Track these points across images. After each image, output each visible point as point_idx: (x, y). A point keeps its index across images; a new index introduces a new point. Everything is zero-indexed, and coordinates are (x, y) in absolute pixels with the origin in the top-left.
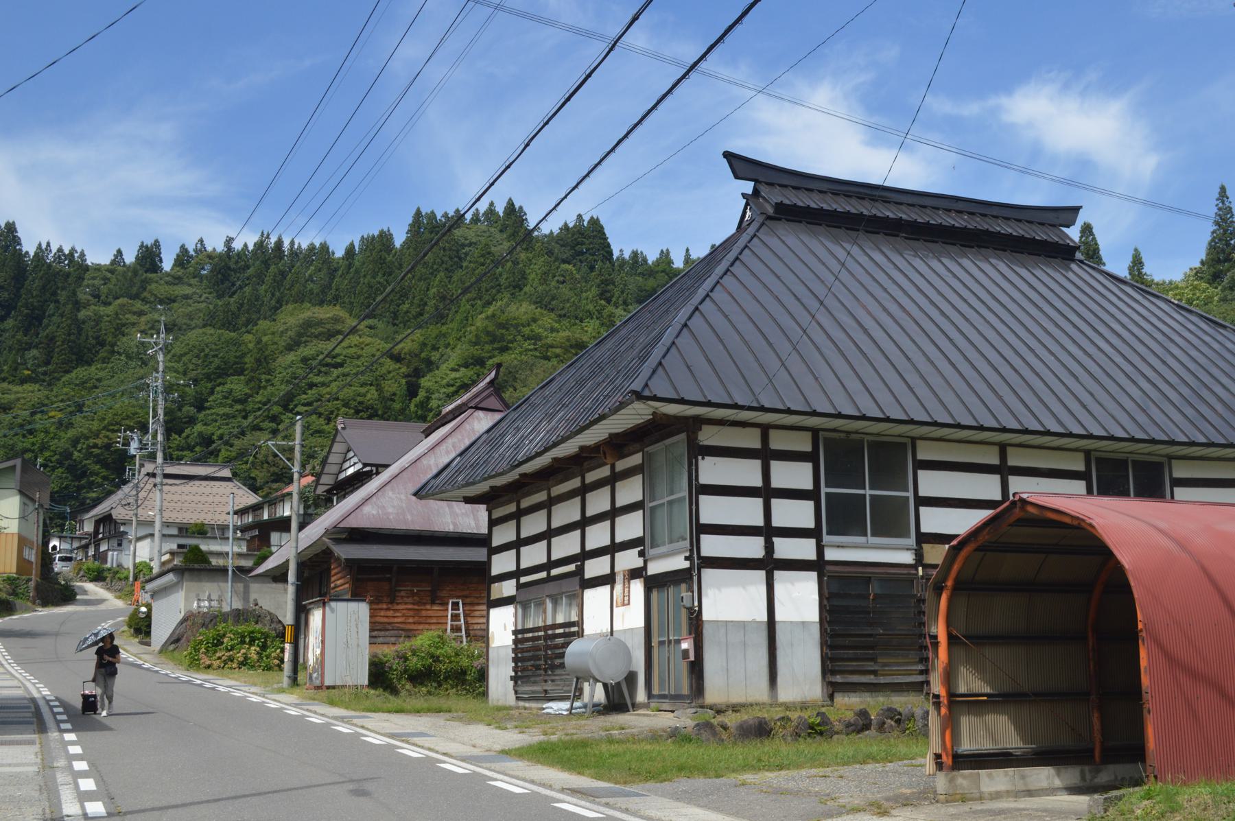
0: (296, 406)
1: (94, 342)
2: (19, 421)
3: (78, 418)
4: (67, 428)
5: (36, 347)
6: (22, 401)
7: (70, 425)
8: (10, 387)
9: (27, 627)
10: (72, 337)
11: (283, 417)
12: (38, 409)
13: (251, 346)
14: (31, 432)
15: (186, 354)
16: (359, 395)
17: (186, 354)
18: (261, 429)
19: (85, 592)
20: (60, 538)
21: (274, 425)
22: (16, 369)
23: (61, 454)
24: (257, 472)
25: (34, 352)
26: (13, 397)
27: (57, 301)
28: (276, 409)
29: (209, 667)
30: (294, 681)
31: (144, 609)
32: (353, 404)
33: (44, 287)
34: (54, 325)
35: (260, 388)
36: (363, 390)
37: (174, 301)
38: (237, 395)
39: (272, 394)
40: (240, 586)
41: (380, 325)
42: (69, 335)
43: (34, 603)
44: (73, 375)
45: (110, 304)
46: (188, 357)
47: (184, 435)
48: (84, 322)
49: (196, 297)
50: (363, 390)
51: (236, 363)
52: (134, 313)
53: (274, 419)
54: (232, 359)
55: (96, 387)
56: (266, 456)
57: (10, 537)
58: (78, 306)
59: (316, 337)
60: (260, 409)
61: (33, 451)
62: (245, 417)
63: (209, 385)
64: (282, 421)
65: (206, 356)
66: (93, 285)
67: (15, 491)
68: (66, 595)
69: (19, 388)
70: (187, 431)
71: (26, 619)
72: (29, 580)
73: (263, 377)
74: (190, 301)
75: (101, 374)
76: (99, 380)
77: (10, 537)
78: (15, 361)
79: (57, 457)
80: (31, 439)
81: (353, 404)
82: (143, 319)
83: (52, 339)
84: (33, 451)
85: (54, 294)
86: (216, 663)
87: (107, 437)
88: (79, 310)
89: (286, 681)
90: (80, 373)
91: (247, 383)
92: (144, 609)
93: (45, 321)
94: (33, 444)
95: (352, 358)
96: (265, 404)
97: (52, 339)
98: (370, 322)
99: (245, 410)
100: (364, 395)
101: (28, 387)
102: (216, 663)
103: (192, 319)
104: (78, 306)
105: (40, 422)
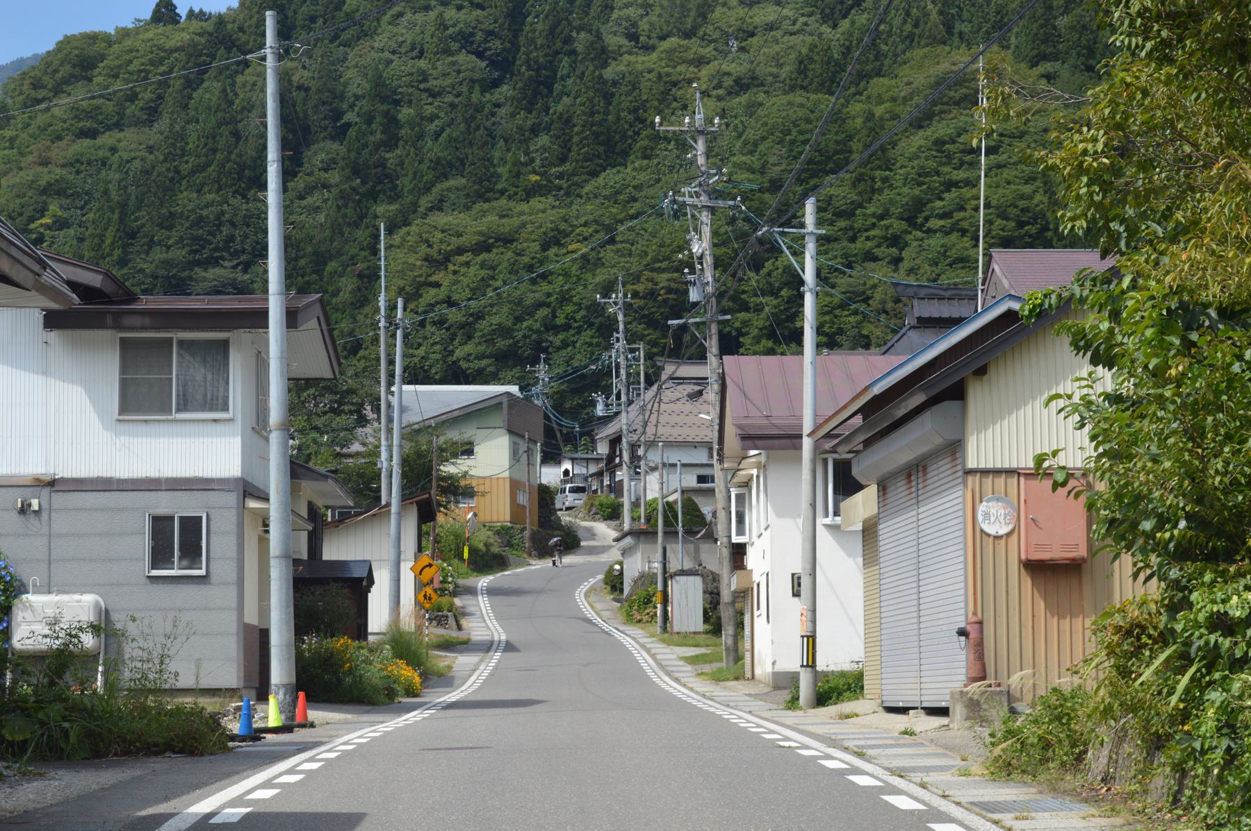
0: (927, 219)
1: (631, 117)
2: (526, 259)
3: (608, 253)
4: (595, 265)
5: (548, 129)
6: (529, 228)
7: (599, 263)
8: (512, 204)
9: (515, 585)
10: (597, 118)
11: (908, 237)
12: (553, 240)
13: (859, 121)
14: (544, 276)
15: (763, 139)
16: (1022, 197)
17: (763, 139)
18: (875, 259)
19: (592, 535)
20: (573, 460)
21: (894, 251)
22: (518, 175)
23: (588, 308)
24: (872, 327)
25: (543, 140)
26: (516, 221)
27: (573, 53)
28: (897, 225)
29: (640, 621)
30: (664, 629)
31: (617, 567)
32: (1013, 212)
33: (552, 31)
34: (570, 100)
35: (873, 191)
36: (1027, 189)
37: (752, 35)
38: (840, 204)
39: (891, 202)
40: (691, 547)
41: (1065, 71)
42: (592, 114)
43: (530, 555)
44: (600, 180)
45: (653, 48)
46: (768, 143)
47: (764, 271)
48: (615, 83)
49: (786, 25)
50: (1027, 189)
51: (837, 152)
52: (690, 62)
53: (895, 241)
54: (832, 146)
55: (635, 200)
56: (884, 302)
57: (501, 482)
58: (603, 56)
59: (957, 103)
60: (874, 225)
61: (548, 305)
62: (853, 239)
63: (799, 189)
64: (906, 244)
65: (793, 142)
66: (628, 19)
67: (504, 431)
68: (570, 542)
69: (524, 207)
70: (768, 265)
71: (518, 575)
72: (523, 530)
73: (878, 173)
74: (778, 34)
75: (642, 177)
76: (638, 188)
77: (501, 482)
78: (516, 163)
79: (583, 313)
80: (545, 287)
81: (1013, 212)
82: (705, 72)
83: (567, 122)
84: (548, 305)
85: (568, 40)
86: (645, 618)
87: (652, 280)
88: (605, 65)
89: (659, 630)
90: (610, 178)
91: (854, 185)
92: (617, 567)
93: (557, 87)
94: (549, 295)
95: (1012, 136)
96: (881, 217)
97: (567, 122)
98: (1048, 67)
99: (852, 228)
100: (1030, 198)
101: (536, 203)
102: (645, 618)
103: (781, 66)
104: (603, 56)
105: (559, 260)
